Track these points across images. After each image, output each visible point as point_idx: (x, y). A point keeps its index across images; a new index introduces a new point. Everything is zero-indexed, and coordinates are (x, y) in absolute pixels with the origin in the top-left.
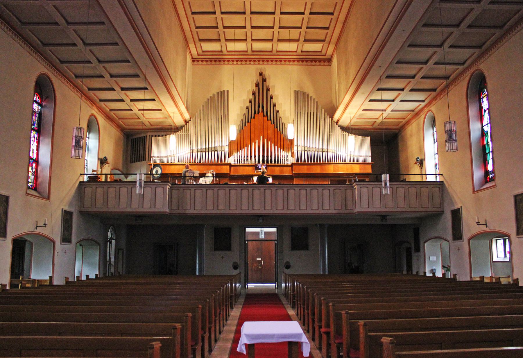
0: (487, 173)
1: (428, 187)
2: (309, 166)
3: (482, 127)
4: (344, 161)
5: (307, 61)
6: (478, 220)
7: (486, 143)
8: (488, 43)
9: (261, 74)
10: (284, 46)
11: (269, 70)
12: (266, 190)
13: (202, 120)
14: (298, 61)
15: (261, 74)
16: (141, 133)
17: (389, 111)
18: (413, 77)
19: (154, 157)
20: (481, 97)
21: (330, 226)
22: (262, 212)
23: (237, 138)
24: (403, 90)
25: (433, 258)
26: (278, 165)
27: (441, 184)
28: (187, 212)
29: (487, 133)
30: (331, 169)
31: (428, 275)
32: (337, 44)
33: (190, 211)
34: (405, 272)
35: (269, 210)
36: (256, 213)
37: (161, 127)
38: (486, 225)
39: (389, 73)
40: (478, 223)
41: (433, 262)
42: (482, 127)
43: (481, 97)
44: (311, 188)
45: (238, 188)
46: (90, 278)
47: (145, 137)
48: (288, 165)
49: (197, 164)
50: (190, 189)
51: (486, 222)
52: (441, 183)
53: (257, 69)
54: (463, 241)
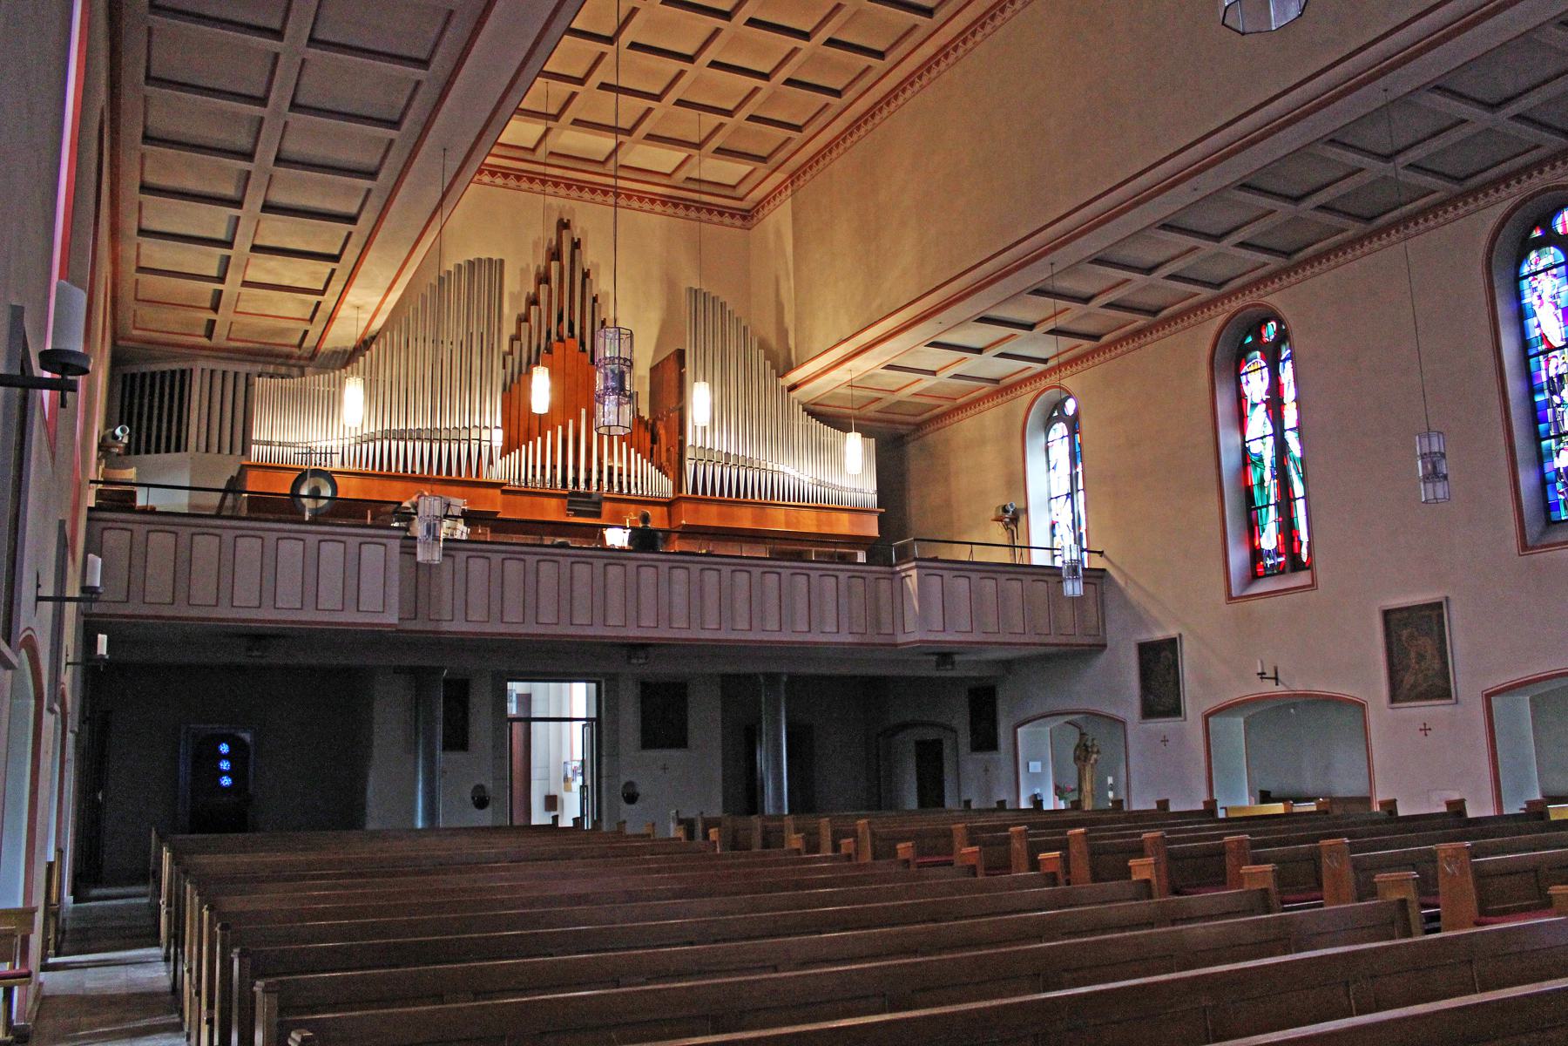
0: (1257, 554)
1: (591, 564)
2: (725, 509)
3: (1244, 442)
4: (804, 501)
5: (687, 208)
6: (1263, 668)
7: (1255, 482)
8: (1310, 251)
9: (564, 225)
10: (642, 155)
11: (590, 218)
12: (644, 568)
13: (420, 342)
14: (664, 203)
15: (564, 225)
16: (155, 359)
17: (943, 376)
18: (1086, 300)
19: (258, 442)
20: (1243, 371)
21: (793, 679)
22: (632, 632)
23: (551, 409)
24: (1030, 327)
25: (1035, 767)
26: (543, 491)
27: (1098, 577)
28: (445, 627)
29: (1261, 460)
30: (778, 522)
31: (1048, 805)
32: (794, 177)
33: (455, 625)
34: (912, 802)
35: (583, 624)
36: (623, 638)
37: (257, 346)
38: (1276, 679)
40: (1262, 675)
41: (1035, 775)
42: (1244, 442)
43: (1243, 371)
44: (671, 564)
45: (594, 561)
47: (183, 372)
48: (657, 500)
49: (397, 477)
50: (453, 556)
51: (1276, 673)
52: (1100, 574)
53: (547, 208)
54: (1185, 719)
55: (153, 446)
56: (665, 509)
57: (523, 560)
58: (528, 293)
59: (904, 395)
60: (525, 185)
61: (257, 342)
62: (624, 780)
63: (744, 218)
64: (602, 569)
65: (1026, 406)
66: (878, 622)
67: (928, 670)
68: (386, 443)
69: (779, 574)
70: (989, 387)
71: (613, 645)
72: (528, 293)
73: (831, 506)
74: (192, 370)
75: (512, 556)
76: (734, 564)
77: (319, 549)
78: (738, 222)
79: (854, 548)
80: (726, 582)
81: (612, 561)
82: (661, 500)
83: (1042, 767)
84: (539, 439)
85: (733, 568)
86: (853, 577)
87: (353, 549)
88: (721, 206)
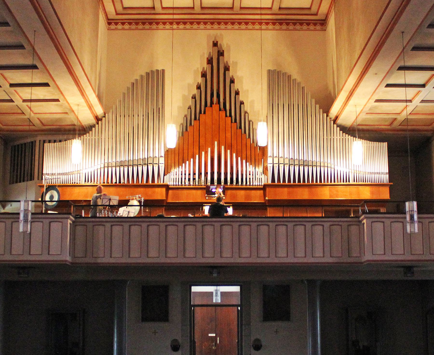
2: (291, 189)
4: (346, 181)
5: (288, 24)
9: (215, 44)
15: (215, 44)
17: (417, 102)
21: (324, 283)
22: (218, 260)
23: (178, 144)
28: (99, 261)
33: (105, 260)
37: (58, 127)
47: (32, 142)
48: (259, 187)
49: (116, 186)
53: (209, 36)
58: (198, 83)
59: (404, 115)
60: (305, 27)
62: (253, 339)
66: (349, 250)
67: (400, 277)
68: (118, 169)
72: (198, 83)
76: (112, 222)
79: (378, 206)
80: (272, 232)
81: (114, 223)
85: (221, 223)
86: (333, 225)
87: (9, 225)
88: (122, 20)
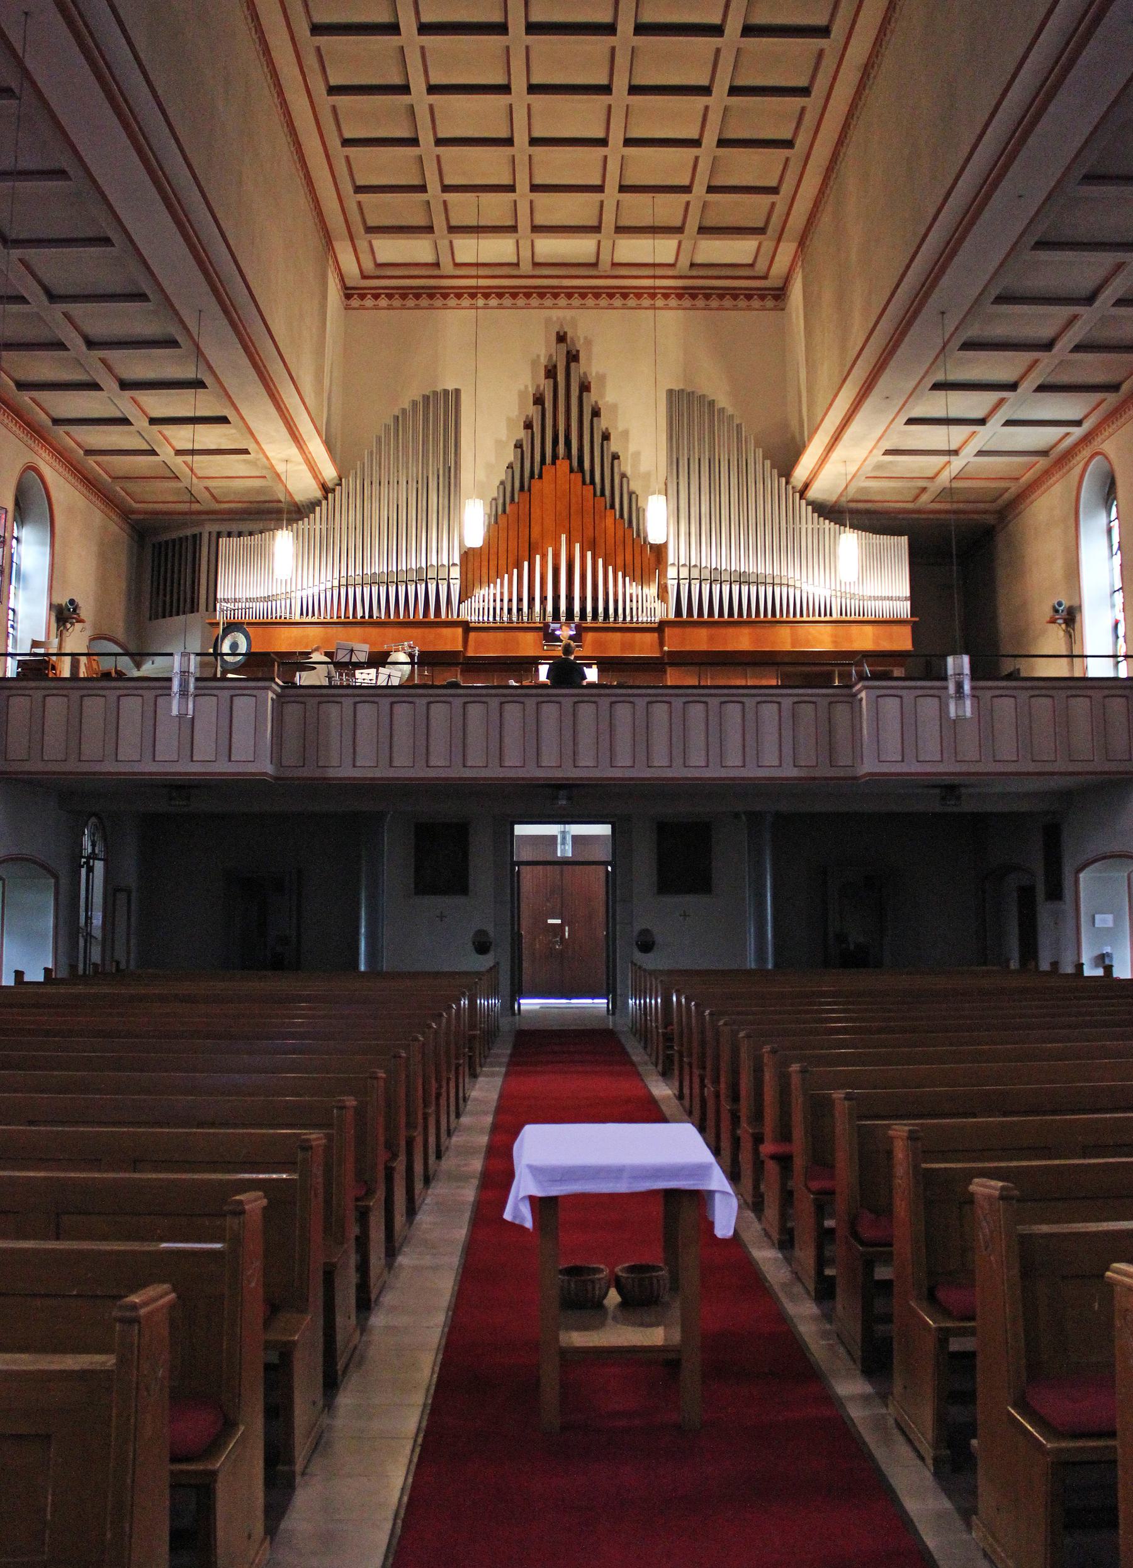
2: (714, 631)
13: (375, 485)
15: (561, 338)
18: (1048, 346)
24: (1013, 387)
26: (511, 625)
28: (332, 773)
30: (784, 641)
31: (1088, 972)
33: (345, 771)
39: (972, 332)
46: (27, 979)
47: (194, 536)
53: (548, 321)
55: (168, 611)
56: (656, 635)
57: (450, 703)
61: (239, 502)
62: (638, 927)
63: (777, 298)
64: (425, 708)
65: (1077, 478)
69: (779, 703)
70: (1042, 463)
71: (542, 786)
73: (848, 618)
74: (201, 534)
75: (438, 699)
77: (156, 704)
78: (770, 303)
82: (649, 625)
83: (1115, 921)
84: (506, 576)
